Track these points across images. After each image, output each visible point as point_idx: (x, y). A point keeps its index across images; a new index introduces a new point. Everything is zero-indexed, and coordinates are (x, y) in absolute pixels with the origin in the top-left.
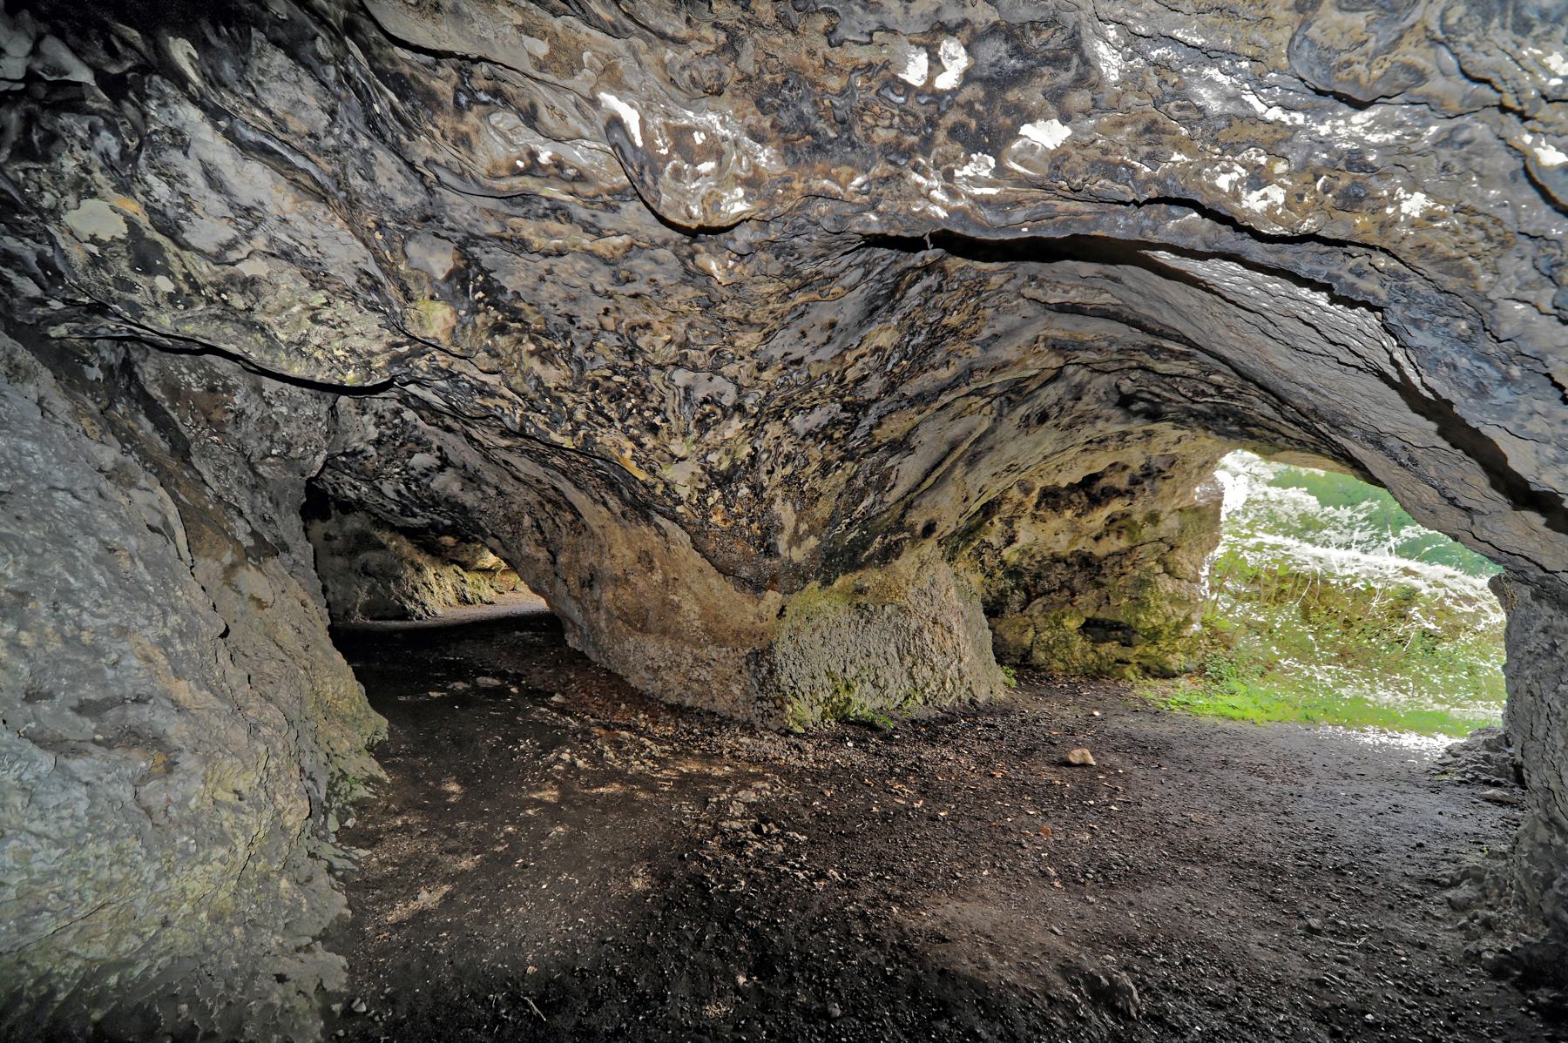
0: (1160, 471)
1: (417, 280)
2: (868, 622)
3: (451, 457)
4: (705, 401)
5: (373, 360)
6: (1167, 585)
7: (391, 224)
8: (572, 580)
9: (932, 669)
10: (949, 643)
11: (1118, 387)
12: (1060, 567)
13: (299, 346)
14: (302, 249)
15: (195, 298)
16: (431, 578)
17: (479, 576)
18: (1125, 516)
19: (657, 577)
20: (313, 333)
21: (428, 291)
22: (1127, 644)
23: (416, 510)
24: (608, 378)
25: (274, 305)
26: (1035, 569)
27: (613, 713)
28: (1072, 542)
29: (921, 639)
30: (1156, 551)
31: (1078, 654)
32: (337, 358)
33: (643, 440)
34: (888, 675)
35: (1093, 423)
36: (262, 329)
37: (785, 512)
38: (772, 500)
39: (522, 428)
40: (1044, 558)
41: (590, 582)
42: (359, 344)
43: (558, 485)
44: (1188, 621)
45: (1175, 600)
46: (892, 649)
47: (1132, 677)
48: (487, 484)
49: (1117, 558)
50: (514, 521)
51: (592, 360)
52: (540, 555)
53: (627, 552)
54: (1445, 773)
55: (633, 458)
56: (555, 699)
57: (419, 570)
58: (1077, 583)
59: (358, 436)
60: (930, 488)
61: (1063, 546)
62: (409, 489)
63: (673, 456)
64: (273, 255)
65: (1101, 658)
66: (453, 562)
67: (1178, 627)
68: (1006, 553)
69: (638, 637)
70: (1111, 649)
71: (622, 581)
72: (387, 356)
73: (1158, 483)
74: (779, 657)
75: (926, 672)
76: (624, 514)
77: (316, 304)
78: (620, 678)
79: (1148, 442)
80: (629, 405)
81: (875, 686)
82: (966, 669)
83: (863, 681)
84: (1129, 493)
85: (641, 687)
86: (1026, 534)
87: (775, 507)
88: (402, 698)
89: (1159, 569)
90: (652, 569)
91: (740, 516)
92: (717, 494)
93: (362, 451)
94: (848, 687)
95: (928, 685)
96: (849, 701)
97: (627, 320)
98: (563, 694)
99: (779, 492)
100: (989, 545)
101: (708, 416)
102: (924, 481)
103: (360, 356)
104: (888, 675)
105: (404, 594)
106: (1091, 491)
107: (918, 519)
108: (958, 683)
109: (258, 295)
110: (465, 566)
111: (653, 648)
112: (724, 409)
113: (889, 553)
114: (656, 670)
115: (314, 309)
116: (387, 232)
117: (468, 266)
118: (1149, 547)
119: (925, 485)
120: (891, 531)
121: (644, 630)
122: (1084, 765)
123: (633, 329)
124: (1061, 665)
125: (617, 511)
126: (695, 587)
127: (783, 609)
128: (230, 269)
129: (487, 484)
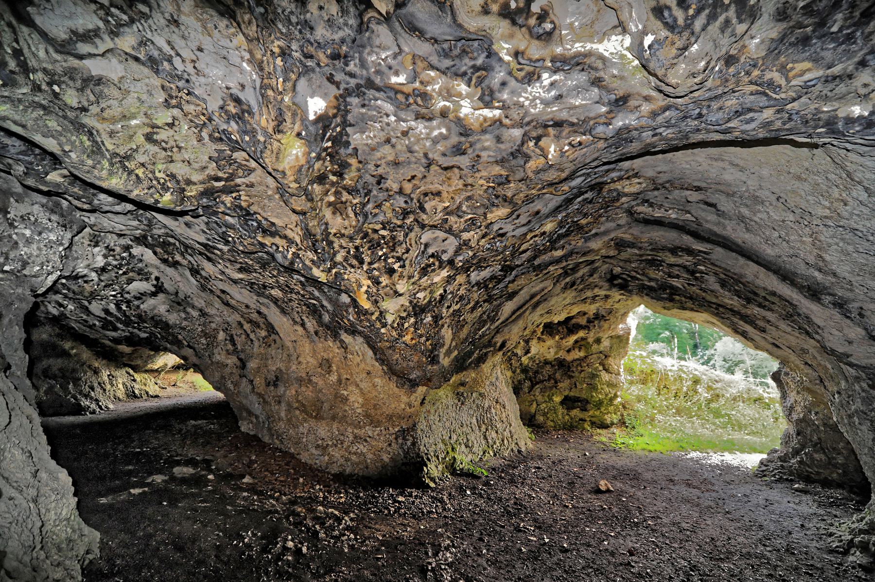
0: (603, 316)
1: (294, 115)
2: (462, 404)
3: (166, 286)
4: (433, 256)
5: (188, 188)
6: (605, 376)
7: (296, 55)
8: (258, 381)
9: (497, 432)
10: (504, 415)
11: (612, 271)
12: (548, 367)
13: (122, 160)
14: (177, 61)
15: (20, 79)
16: (106, 378)
17: (146, 376)
18: (583, 339)
19: (334, 378)
20: (141, 150)
21: (297, 128)
22: (584, 409)
23: (119, 325)
24: (376, 231)
25: (115, 110)
26: (535, 368)
27: (295, 487)
28: (556, 353)
29: (490, 413)
30: (599, 358)
31: (560, 417)
32: (157, 179)
33: (381, 279)
34: (473, 438)
35: (593, 289)
36: (91, 134)
37: (447, 333)
38: (443, 326)
39: (292, 263)
40: (540, 362)
41: (275, 381)
42: (181, 170)
43: (263, 310)
44: (616, 396)
45: (610, 385)
46: (474, 421)
47: (589, 428)
48: (193, 307)
49: (578, 362)
50: (211, 337)
51: (376, 215)
52: (229, 361)
53: (311, 360)
54: (765, 476)
55: (367, 292)
56: (245, 480)
57: (96, 372)
58: (558, 376)
59: (86, 263)
60: (513, 321)
61: (551, 355)
62: (118, 307)
63: (396, 292)
64: (137, 59)
65: (572, 419)
66: (125, 365)
67: (611, 400)
68: (523, 359)
69: (313, 423)
70: (576, 412)
71: (305, 381)
72: (201, 188)
73: (602, 323)
74: (419, 432)
75: (494, 434)
76: (316, 333)
77: (159, 123)
78: (292, 456)
79: (606, 301)
80: (380, 253)
81: (467, 446)
82: (513, 431)
83: (460, 444)
84: (586, 327)
85: (309, 462)
86: (535, 348)
87: (443, 330)
88: (103, 500)
89: (601, 368)
90: (329, 372)
91: (421, 336)
92: (412, 320)
93: (85, 276)
94: (453, 449)
95: (495, 443)
96: (454, 459)
97: (422, 188)
98: (250, 475)
99: (448, 320)
100: (516, 355)
101: (430, 266)
102: (511, 317)
103: (178, 182)
104: (473, 438)
105: (81, 393)
106: (569, 326)
107: (499, 340)
108: (510, 440)
109: (99, 97)
110: (136, 369)
111: (323, 430)
112: (441, 262)
113: (482, 359)
114: (325, 448)
115: (154, 126)
116: (290, 61)
117: (335, 116)
118: (595, 356)
119: (511, 320)
120: (485, 347)
121: (318, 417)
122: (608, 491)
123: (426, 195)
124: (552, 424)
125: (312, 330)
126: (363, 385)
127: (424, 399)
128: (74, 62)
129: (193, 307)
